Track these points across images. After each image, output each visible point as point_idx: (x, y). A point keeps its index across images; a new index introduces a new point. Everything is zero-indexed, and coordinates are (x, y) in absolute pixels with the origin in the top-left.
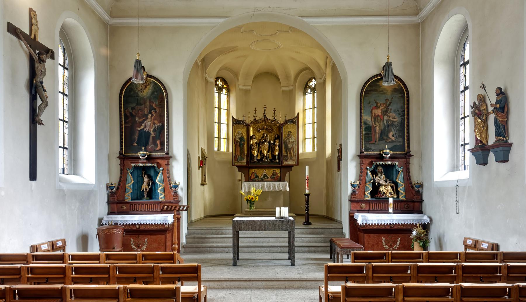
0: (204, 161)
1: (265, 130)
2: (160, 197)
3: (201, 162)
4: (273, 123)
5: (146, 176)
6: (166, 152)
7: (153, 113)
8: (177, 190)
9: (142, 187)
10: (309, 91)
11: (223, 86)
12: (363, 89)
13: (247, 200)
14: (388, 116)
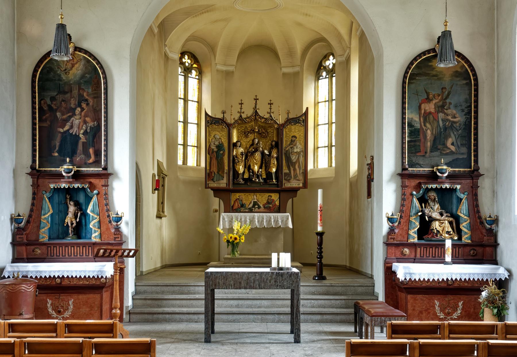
0: (161, 180)
1: (256, 134)
2: (93, 235)
3: (158, 181)
4: (269, 122)
5: (72, 203)
6: (103, 167)
7: (84, 105)
8: (120, 224)
9: (66, 221)
10: (324, 74)
11: (192, 65)
12: (406, 72)
13: (228, 241)
14: (445, 114)
